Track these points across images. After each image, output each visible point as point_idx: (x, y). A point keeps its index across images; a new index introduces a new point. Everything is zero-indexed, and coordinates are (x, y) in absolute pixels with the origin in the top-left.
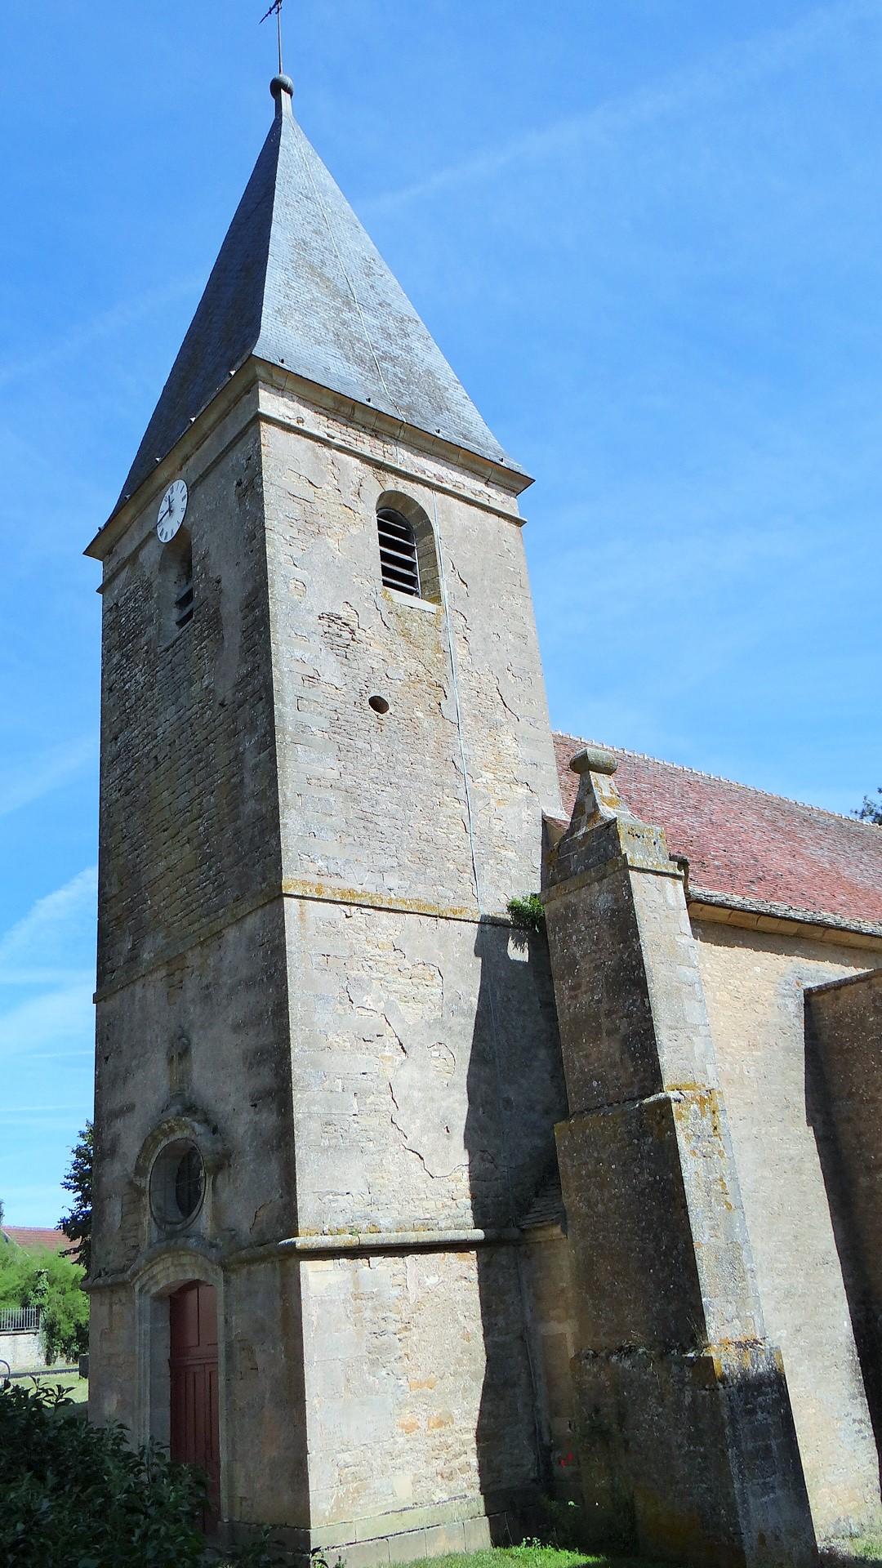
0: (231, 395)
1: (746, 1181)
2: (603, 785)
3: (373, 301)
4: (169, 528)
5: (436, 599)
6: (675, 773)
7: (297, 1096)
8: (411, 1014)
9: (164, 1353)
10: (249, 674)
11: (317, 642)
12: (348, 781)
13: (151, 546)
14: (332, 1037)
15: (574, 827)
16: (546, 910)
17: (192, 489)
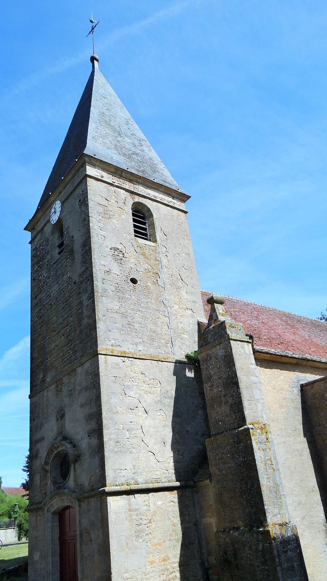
0: (76, 168)
2: (219, 308)
3: (129, 134)
4: (55, 218)
5: (155, 241)
6: (248, 305)
7: (105, 432)
8: (149, 399)
9: (57, 536)
11: (110, 258)
12: (123, 310)
13: (48, 225)
14: (118, 408)
15: (209, 324)
17: (63, 203)
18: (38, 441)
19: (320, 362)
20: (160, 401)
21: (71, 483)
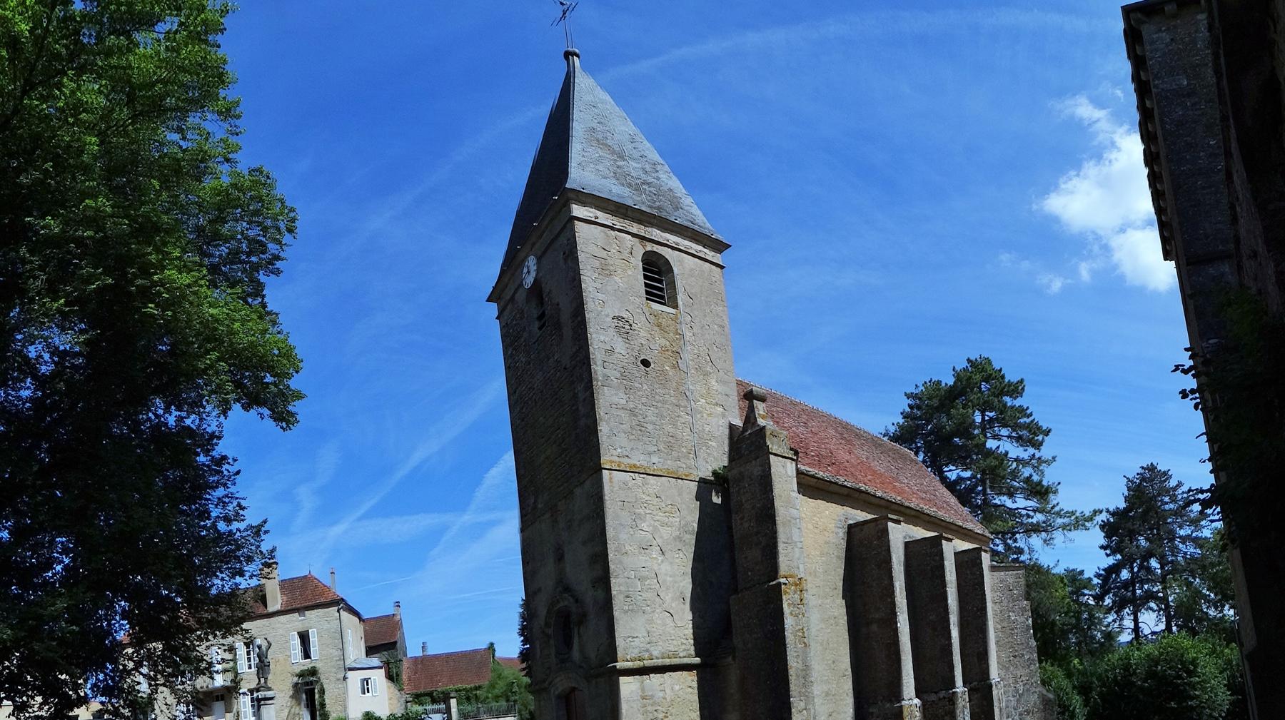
1: (813, 631)
2: (760, 407)
3: (636, 154)
4: (529, 280)
5: (676, 307)
6: (796, 404)
7: (613, 581)
8: (666, 533)
10: (578, 351)
11: (612, 332)
12: (631, 405)
13: (521, 290)
14: (628, 547)
15: (745, 429)
16: (730, 475)
17: (539, 260)
18: (535, 593)
19: (874, 496)
20: (679, 538)
21: (576, 654)
